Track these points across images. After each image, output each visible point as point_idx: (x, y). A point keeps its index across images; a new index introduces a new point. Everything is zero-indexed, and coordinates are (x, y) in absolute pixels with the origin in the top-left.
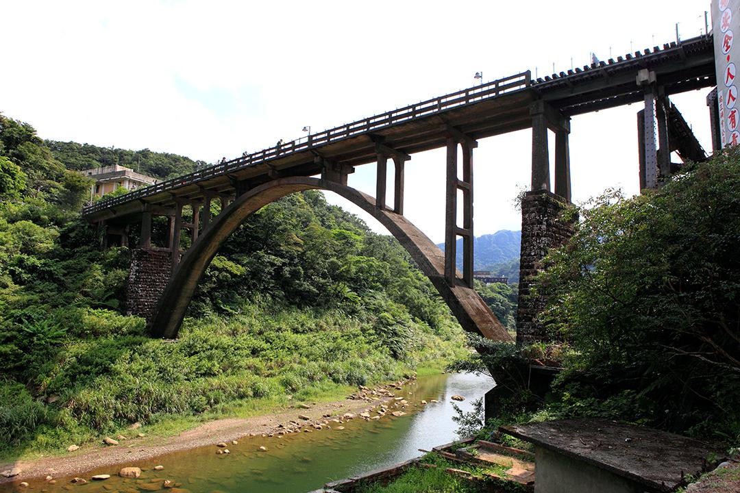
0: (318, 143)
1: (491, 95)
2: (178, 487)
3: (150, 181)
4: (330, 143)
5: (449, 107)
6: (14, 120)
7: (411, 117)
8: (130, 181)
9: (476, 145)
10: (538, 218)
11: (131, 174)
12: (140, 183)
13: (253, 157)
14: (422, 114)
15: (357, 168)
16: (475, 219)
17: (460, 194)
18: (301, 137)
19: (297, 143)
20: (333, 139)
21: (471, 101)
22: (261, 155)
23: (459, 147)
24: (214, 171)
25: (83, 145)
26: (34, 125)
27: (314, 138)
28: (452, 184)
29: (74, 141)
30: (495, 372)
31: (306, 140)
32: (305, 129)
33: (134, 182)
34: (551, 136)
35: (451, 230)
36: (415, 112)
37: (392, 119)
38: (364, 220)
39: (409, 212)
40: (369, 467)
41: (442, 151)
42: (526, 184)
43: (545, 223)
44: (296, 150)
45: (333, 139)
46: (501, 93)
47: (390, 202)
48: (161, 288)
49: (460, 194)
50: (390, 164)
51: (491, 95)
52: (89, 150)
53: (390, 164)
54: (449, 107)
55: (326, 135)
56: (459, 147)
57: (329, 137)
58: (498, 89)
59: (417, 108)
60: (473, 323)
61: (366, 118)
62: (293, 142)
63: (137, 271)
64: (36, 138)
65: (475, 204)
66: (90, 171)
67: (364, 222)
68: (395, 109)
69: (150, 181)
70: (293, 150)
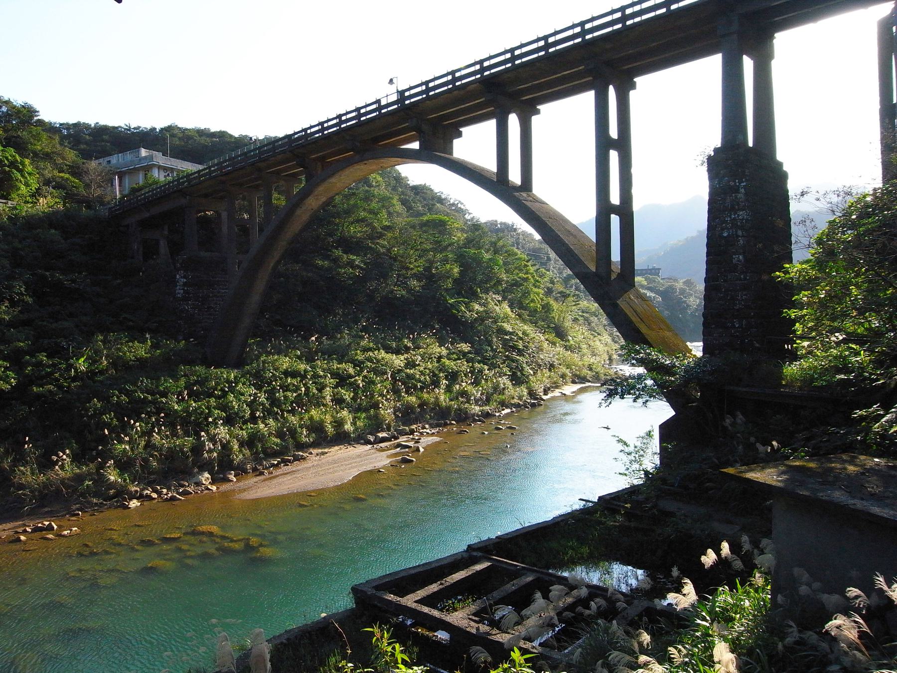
0: (412, 100)
1: (577, 41)
2: (265, 546)
3: (190, 167)
4: (429, 98)
5: (596, 34)
6: (12, 100)
7: (450, 86)
8: (159, 167)
9: (633, 86)
10: (732, 183)
11: (160, 159)
12: (172, 170)
13: (326, 125)
14: (389, 109)
15: (464, 130)
16: (635, 191)
17: (614, 156)
18: (388, 95)
19: (383, 102)
20: (344, 125)
21: (629, 23)
22: (335, 122)
23: (612, 91)
24: (341, 122)
25: (93, 126)
26: (36, 105)
27: (407, 94)
28: (604, 144)
29: (82, 121)
30: (673, 396)
31: (394, 98)
32: (391, 81)
33: (165, 169)
34: (748, 64)
35: (604, 210)
36: (483, 70)
37: (455, 79)
38: (462, 201)
39: (539, 189)
40: (636, 618)
41: (588, 98)
42: (714, 139)
43: (743, 190)
44: (383, 111)
45: (344, 125)
46: (517, 62)
47: (515, 176)
48: (216, 304)
49: (614, 156)
50: (513, 120)
51: (577, 41)
52: (101, 132)
53: (513, 120)
54: (596, 34)
55: (320, 127)
56: (612, 91)
57: (360, 115)
58: (514, 58)
59: (551, 40)
60: (638, 331)
61: (424, 81)
62: (378, 101)
63: (185, 284)
64: (39, 120)
65: (634, 171)
66: (107, 159)
67: (462, 204)
68: (590, 17)
69: (190, 167)
70: (380, 112)
